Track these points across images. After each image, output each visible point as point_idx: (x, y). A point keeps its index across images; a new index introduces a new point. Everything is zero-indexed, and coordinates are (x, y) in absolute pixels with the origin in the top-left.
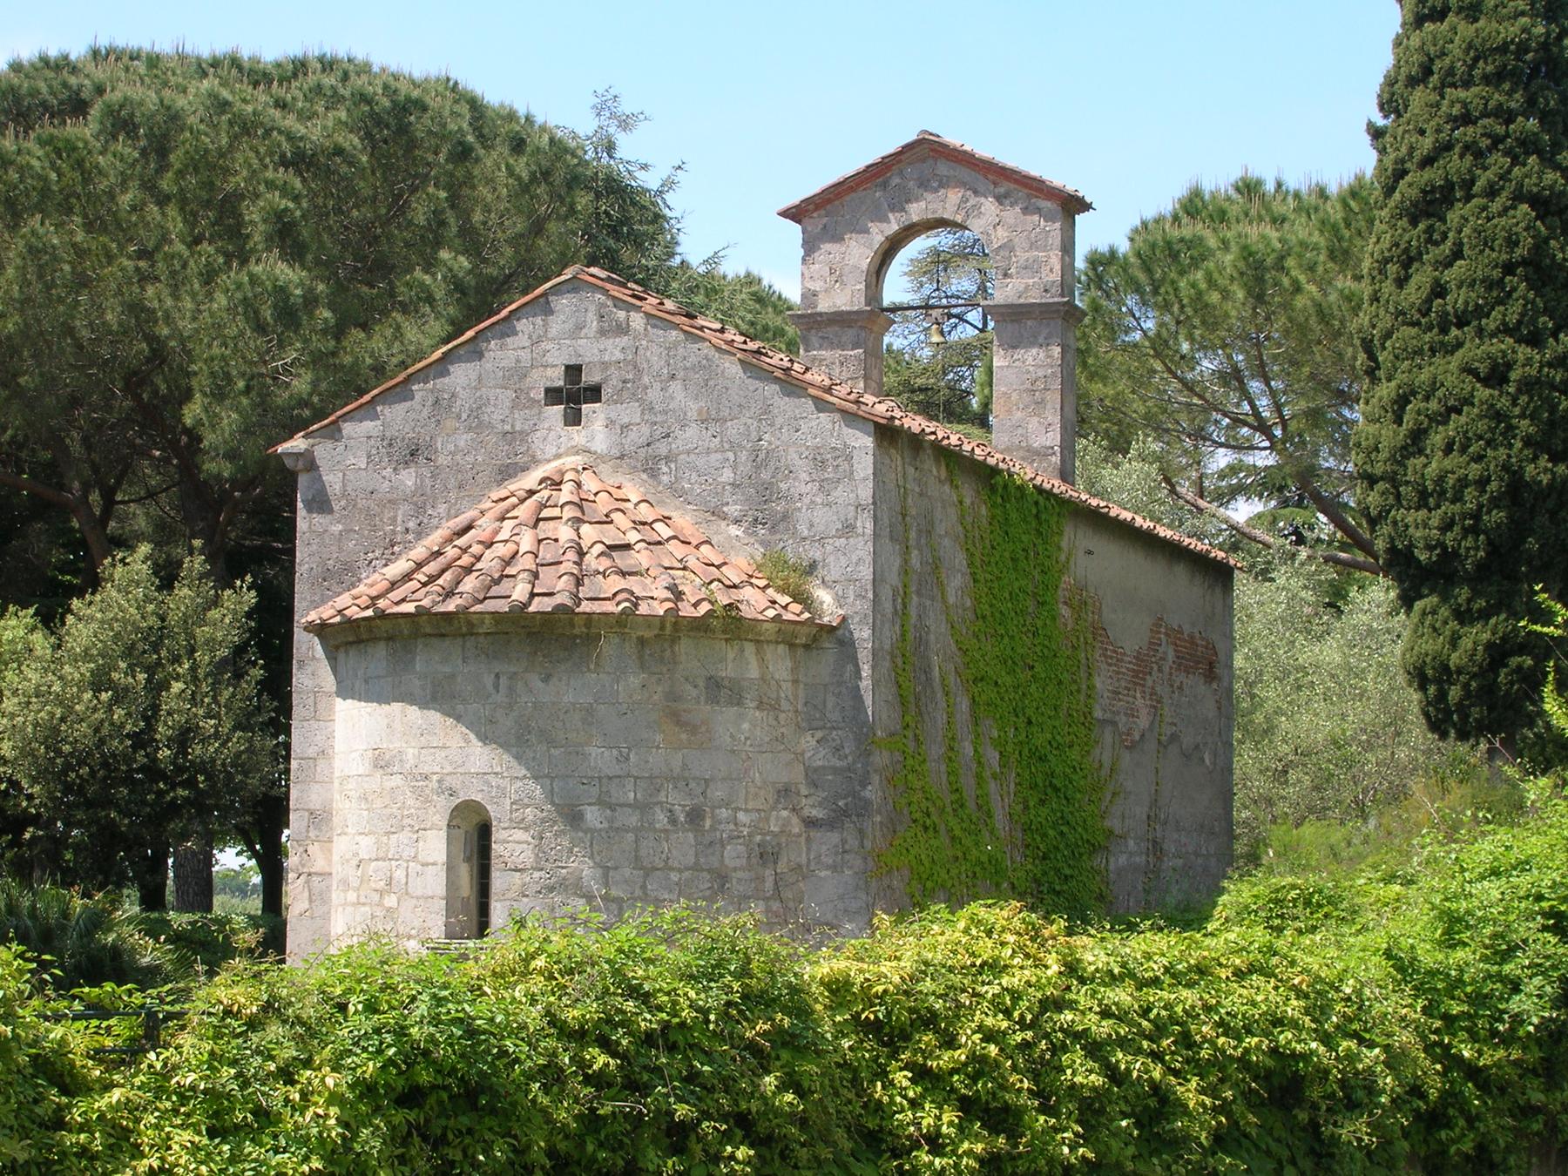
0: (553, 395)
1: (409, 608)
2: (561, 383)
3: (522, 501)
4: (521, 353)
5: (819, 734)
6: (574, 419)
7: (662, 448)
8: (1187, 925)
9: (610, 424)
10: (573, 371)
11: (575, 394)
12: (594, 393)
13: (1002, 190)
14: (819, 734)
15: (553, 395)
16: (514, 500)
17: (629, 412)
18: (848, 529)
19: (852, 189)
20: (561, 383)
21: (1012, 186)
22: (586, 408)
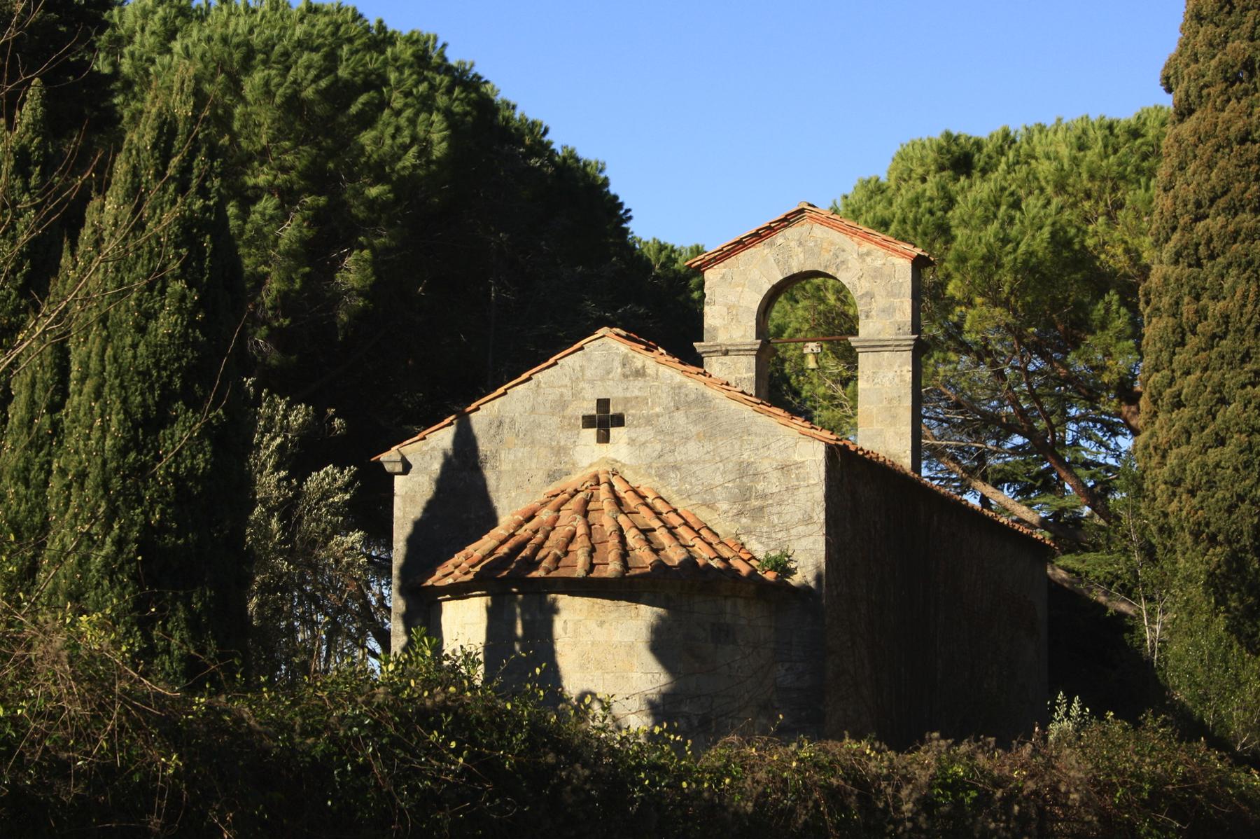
0: (588, 422)
1: (450, 580)
2: (594, 412)
3: (572, 496)
4: (564, 390)
5: (787, 665)
6: (604, 438)
7: (670, 459)
8: (953, 204)
9: (632, 442)
10: (603, 404)
11: (604, 421)
12: (619, 421)
13: (865, 250)
14: (787, 665)
15: (588, 422)
16: (566, 496)
17: (646, 434)
18: (808, 520)
19: (740, 242)
20: (594, 412)
21: (873, 246)
22: (614, 432)
